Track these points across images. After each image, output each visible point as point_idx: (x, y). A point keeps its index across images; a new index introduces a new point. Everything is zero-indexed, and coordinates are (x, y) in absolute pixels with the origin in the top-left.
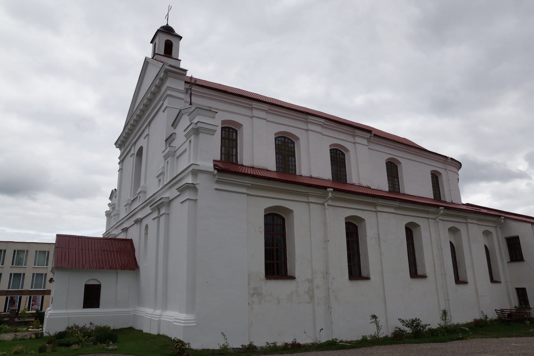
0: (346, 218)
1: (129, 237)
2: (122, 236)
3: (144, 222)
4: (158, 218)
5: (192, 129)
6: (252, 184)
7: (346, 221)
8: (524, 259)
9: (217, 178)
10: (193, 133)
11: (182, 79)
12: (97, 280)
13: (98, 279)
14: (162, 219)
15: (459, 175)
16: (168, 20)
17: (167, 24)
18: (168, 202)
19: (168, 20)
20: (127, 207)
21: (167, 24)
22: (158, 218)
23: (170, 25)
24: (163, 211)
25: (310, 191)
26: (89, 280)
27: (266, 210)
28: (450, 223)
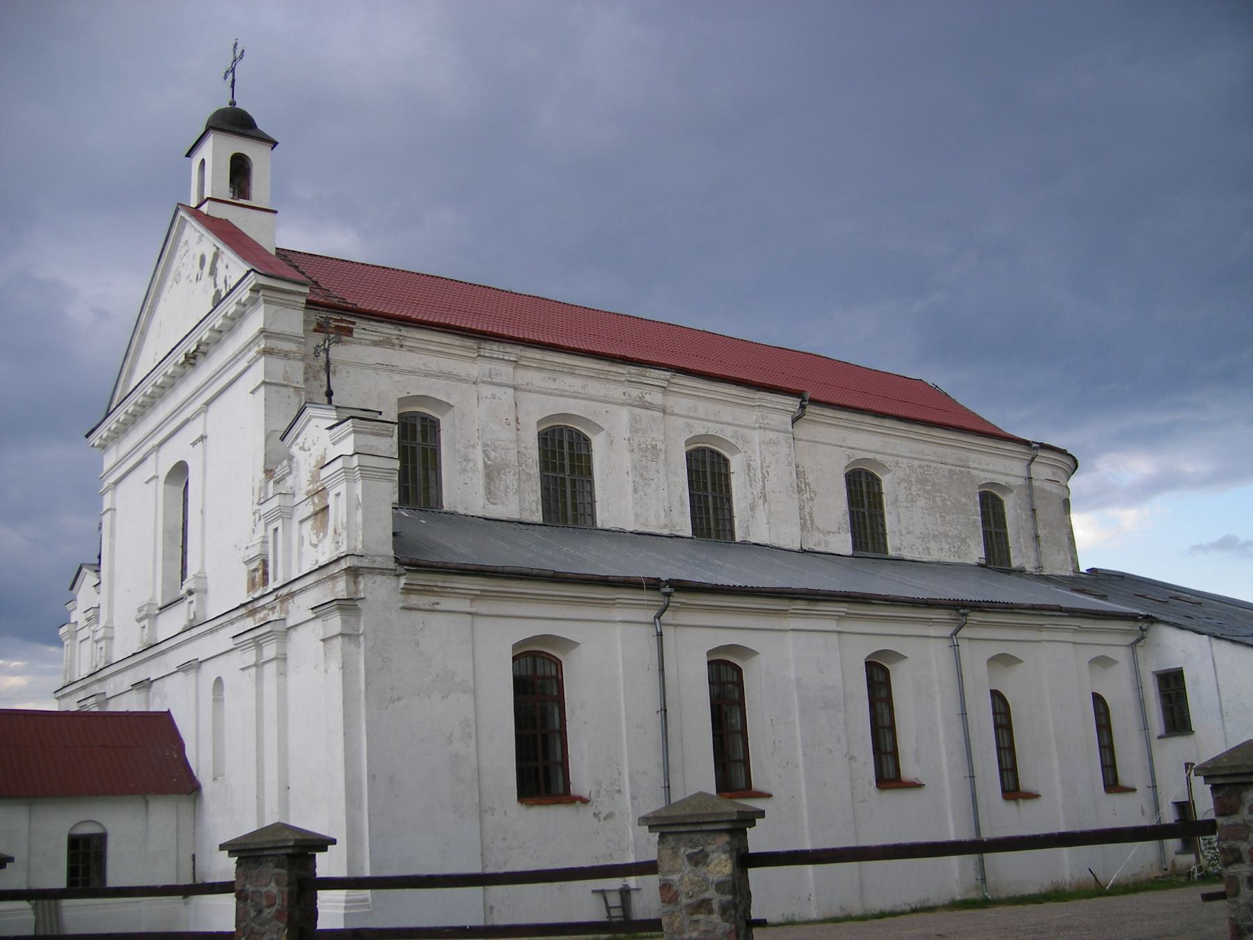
0: (709, 653)
1: (156, 706)
2: (132, 703)
3: (210, 672)
4: (259, 665)
5: (342, 470)
6: (482, 591)
7: (710, 659)
8: (1193, 729)
9: (405, 584)
10: (255, 290)
11: (296, 306)
12: (98, 823)
13: (99, 821)
14: (270, 669)
15: (1071, 492)
16: (233, 86)
17: (233, 103)
18: (283, 632)
19: (233, 86)
20: (145, 622)
21: (233, 103)
22: (259, 665)
23: (240, 105)
24: (270, 650)
25: (618, 596)
26: (78, 824)
27: (515, 647)
28: (993, 644)
